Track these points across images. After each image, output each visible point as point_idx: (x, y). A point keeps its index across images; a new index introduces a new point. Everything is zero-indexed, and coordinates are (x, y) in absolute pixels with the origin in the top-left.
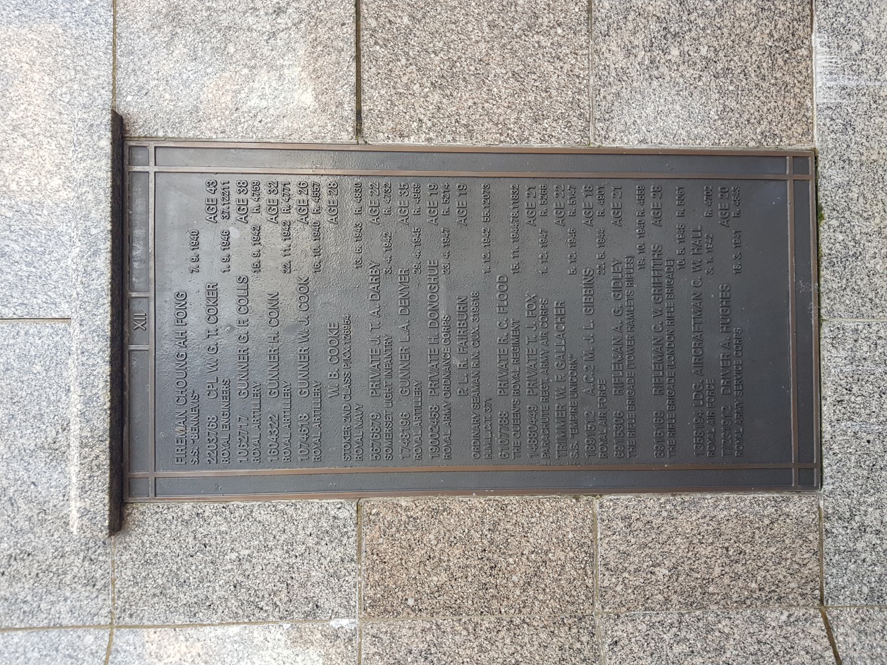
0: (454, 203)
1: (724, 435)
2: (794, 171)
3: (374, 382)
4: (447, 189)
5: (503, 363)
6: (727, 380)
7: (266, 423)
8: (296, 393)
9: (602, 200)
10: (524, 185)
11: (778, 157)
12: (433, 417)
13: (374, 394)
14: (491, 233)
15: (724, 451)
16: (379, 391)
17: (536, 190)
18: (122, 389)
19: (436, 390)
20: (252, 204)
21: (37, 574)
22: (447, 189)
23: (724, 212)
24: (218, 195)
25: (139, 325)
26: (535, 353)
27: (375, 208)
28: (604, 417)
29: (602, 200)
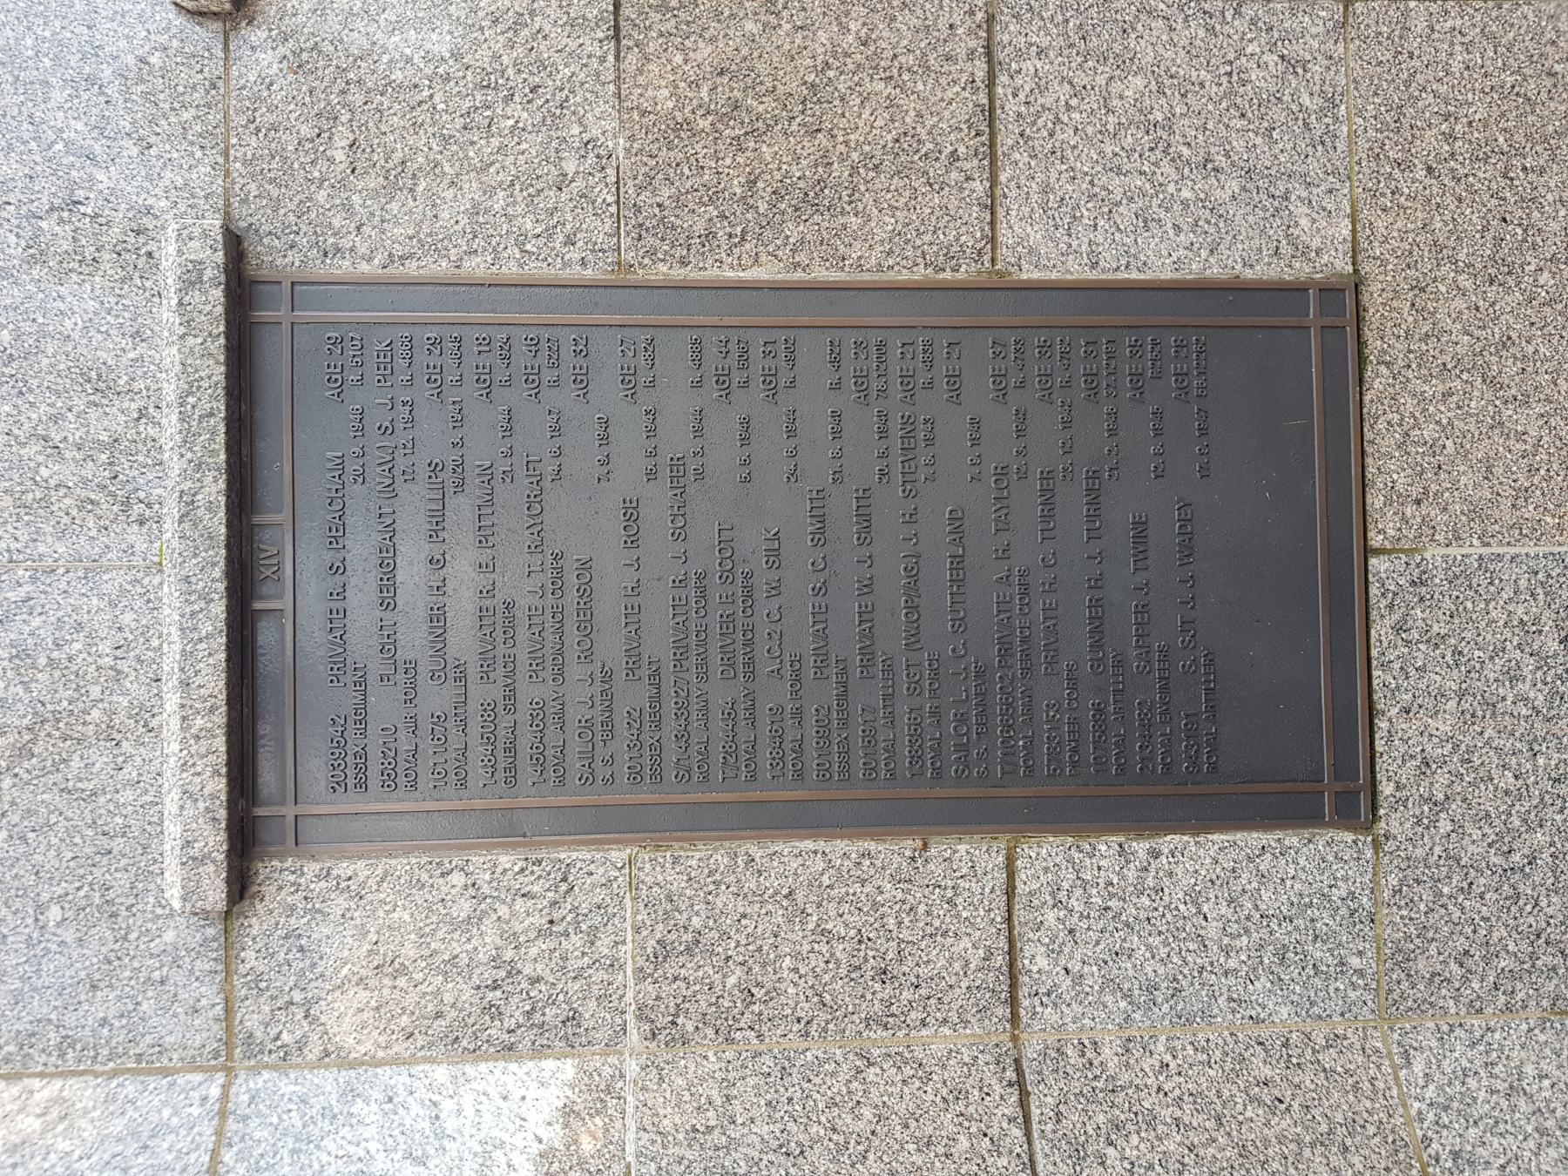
0: (941, 369)
1: (1186, 746)
2: (1322, 312)
3: (630, 657)
4: (929, 347)
5: (632, 628)
6: (681, 650)
7: (425, 726)
8: (372, 679)
9: (930, 364)
10: (851, 338)
11: (1296, 290)
12: (726, 716)
13: (534, 679)
14: (1028, 417)
15: (1002, 768)
16: (491, 675)
17: (776, 346)
18: (243, 668)
19: (490, 674)
20: (500, 375)
21: (538, 980)
22: (929, 347)
23: (1135, 378)
24: (543, 359)
25: (268, 573)
26: (870, 609)
27: (861, 379)
28: (798, 713)
29: (930, 364)
